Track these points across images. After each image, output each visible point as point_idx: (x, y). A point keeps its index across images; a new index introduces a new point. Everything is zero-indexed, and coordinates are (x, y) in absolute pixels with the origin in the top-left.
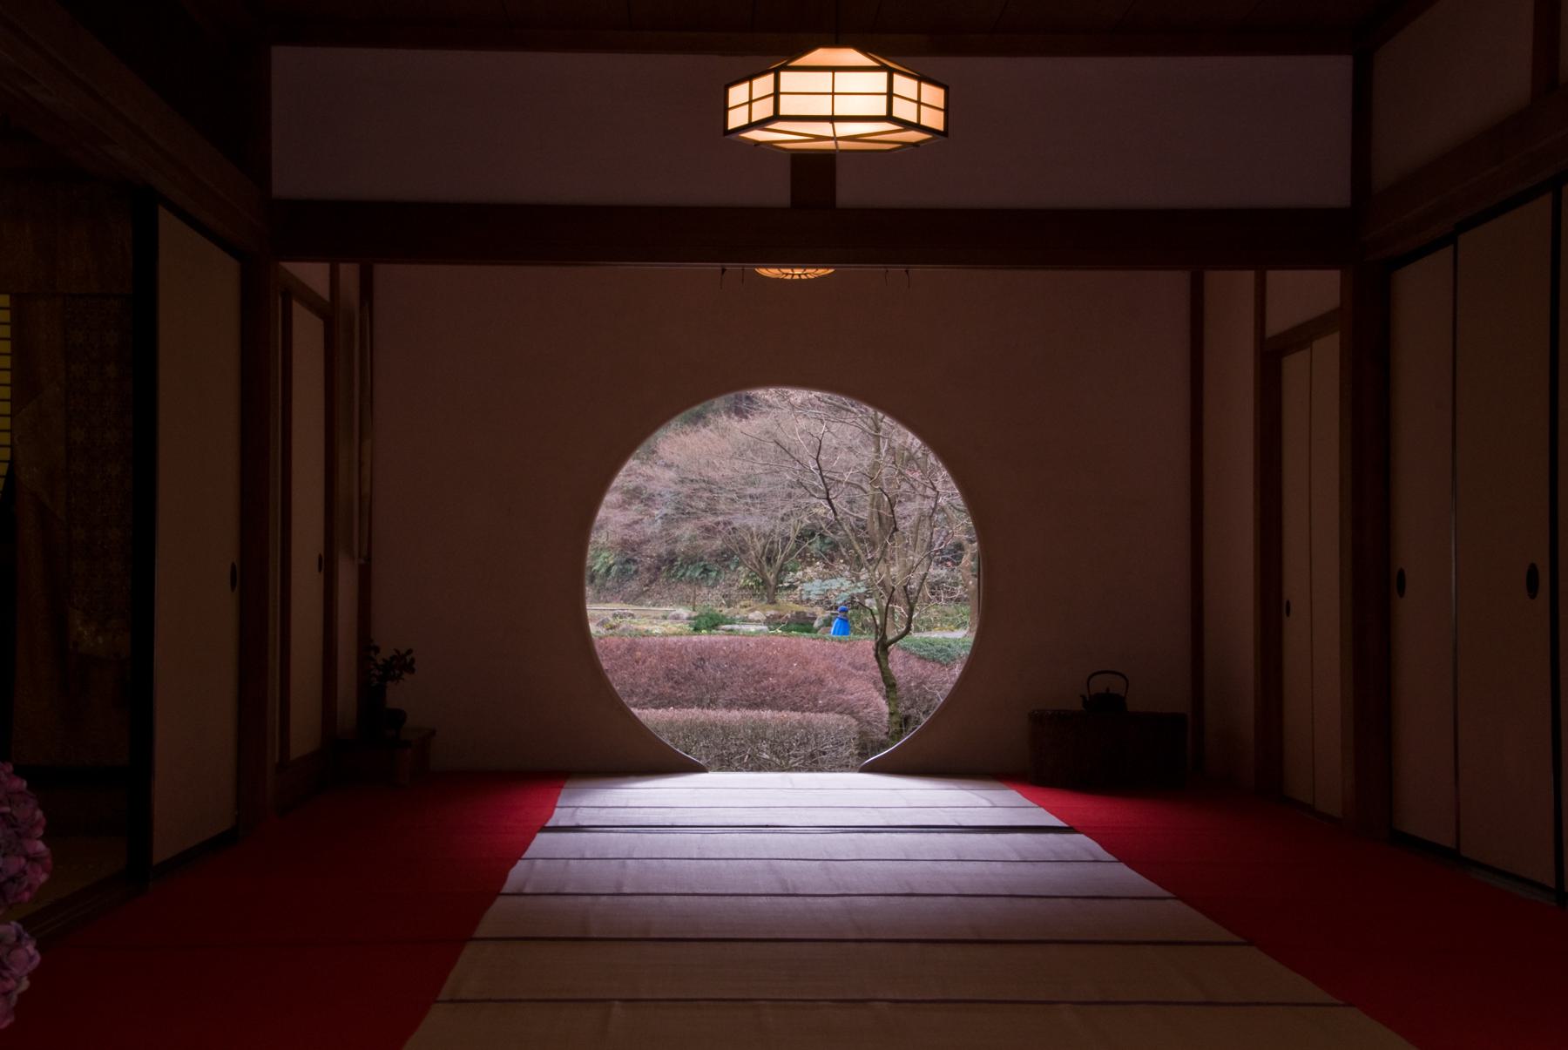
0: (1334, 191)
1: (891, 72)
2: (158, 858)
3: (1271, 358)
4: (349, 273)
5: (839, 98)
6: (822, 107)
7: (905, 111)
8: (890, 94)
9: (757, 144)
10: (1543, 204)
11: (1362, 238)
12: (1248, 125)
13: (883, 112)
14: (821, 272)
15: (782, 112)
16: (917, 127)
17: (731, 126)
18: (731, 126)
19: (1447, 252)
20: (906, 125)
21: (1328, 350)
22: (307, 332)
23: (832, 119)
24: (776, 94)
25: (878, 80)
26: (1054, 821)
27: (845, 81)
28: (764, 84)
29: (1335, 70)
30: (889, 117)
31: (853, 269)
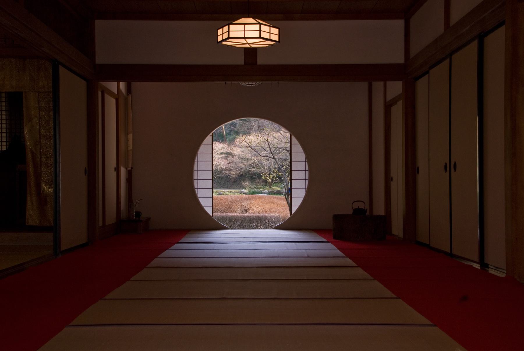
0: (402, 61)
1: (260, 24)
2: (63, 248)
3: (388, 107)
4: (122, 85)
5: (248, 33)
6: (241, 35)
7: (265, 35)
8: (260, 31)
9: (228, 46)
10: (448, 60)
11: (406, 73)
12: (379, 41)
13: (259, 36)
14: (255, 84)
15: (230, 36)
16: (270, 40)
17: (219, 41)
18: (219, 41)
19: (427, 75)
20: (267, 40)
21: (400, 104)
22: (111, 103)
23: (244, 38)
24: (229, 31)
25: (257, 27)
26: (325, 240)
27: (248, 27)
28: (226, 29)
29: (400, 23)
30: (260, 37)
31: (264, 82)
